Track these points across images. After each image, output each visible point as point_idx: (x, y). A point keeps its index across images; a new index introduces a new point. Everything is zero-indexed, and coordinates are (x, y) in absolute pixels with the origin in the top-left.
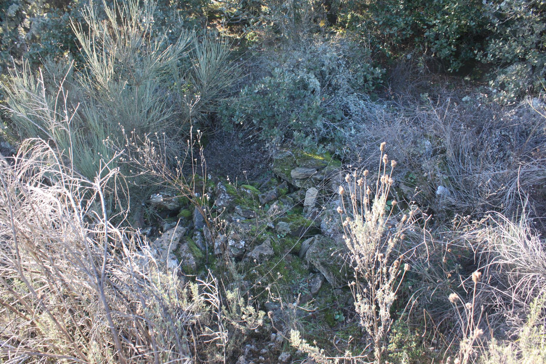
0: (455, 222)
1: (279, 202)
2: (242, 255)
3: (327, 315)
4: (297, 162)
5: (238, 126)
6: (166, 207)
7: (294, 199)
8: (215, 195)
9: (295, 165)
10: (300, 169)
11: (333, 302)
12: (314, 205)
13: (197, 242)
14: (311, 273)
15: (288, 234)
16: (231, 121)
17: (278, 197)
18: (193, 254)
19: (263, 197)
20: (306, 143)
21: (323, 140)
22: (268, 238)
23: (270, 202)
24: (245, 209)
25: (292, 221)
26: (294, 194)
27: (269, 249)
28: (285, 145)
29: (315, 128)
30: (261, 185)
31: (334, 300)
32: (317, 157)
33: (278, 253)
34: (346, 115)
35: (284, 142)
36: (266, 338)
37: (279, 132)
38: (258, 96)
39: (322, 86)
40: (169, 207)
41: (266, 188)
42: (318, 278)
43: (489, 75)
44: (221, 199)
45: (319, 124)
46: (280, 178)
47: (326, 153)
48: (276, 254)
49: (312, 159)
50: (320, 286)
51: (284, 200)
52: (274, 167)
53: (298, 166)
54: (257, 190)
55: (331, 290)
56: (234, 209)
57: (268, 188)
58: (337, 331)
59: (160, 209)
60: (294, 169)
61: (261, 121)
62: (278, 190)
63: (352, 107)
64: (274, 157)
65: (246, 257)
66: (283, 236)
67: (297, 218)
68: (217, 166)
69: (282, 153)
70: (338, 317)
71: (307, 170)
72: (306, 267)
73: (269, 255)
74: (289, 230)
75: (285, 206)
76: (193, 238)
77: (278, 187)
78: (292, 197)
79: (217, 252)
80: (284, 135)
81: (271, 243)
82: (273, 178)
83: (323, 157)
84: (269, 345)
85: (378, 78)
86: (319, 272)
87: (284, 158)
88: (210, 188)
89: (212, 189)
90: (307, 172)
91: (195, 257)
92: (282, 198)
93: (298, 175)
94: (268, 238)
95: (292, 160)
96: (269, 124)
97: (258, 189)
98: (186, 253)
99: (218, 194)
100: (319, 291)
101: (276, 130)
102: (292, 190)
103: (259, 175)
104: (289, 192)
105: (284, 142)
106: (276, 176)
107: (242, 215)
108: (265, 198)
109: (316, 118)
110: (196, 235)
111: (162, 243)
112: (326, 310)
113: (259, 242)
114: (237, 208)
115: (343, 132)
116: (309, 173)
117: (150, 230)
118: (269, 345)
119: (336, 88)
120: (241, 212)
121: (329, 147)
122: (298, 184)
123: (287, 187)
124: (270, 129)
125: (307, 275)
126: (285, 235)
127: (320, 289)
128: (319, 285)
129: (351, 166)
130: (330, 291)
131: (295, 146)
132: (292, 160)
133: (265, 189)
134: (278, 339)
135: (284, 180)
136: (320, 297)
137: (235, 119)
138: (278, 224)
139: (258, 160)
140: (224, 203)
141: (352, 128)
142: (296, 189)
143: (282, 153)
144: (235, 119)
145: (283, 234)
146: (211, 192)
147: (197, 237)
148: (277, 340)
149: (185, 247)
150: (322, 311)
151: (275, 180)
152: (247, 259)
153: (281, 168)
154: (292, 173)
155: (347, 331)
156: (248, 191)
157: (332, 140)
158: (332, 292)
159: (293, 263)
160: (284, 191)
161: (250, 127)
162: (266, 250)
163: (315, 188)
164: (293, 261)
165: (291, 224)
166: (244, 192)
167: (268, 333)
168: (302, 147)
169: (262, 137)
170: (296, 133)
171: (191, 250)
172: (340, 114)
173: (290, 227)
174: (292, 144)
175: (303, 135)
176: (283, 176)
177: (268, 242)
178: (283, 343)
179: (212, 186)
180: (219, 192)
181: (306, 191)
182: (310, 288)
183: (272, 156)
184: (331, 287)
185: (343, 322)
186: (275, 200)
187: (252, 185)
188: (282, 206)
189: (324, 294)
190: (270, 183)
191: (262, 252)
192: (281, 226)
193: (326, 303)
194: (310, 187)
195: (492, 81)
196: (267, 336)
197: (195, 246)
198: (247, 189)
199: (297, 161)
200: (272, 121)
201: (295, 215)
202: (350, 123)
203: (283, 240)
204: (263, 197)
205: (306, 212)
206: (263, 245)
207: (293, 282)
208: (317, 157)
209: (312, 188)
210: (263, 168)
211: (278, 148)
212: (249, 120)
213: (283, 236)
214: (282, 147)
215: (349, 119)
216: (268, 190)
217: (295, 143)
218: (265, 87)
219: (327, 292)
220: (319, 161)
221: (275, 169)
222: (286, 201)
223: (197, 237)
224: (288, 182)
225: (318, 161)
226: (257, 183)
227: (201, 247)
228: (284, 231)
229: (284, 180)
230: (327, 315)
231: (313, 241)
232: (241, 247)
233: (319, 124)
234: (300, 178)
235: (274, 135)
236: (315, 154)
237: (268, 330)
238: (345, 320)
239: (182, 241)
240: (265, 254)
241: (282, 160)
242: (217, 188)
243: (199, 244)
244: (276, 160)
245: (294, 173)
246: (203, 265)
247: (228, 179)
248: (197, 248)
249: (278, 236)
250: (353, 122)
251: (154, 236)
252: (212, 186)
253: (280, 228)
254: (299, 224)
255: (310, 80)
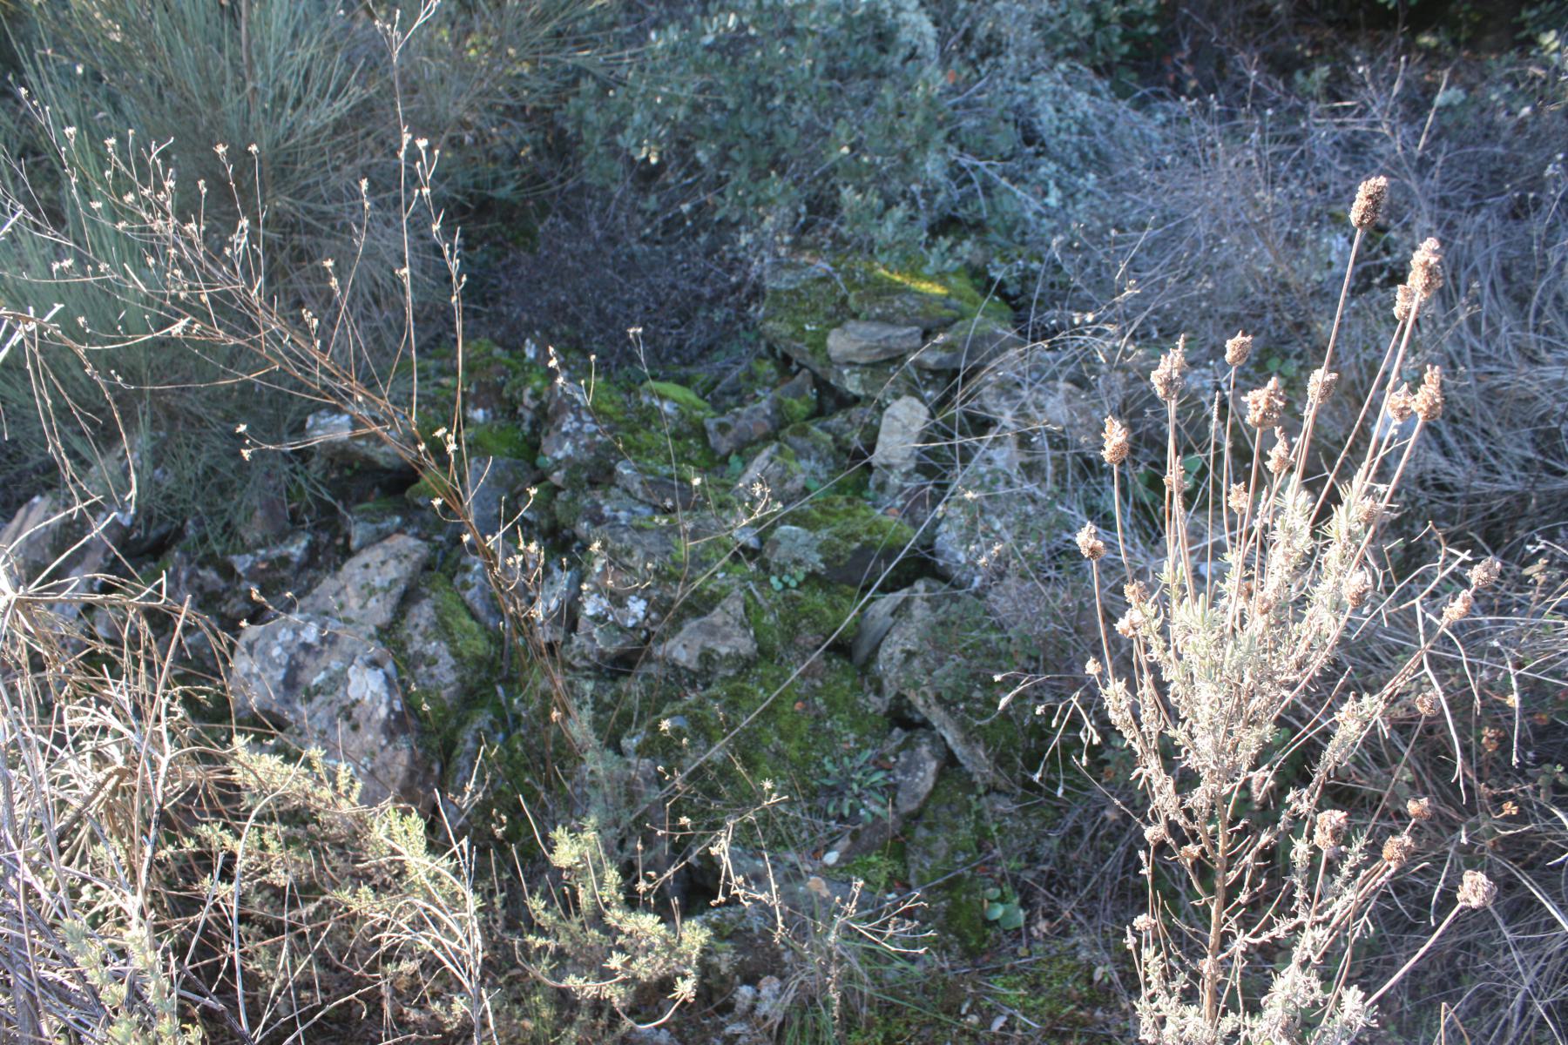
0: (1541, 579)
1: (780, 451)
2: (639, 652)
3: (956, 904)
4: (852, 301)
5: (647, 176)
6: (368, 461)
7: (835, 440)
8: (545, 415)
9: (842, 314)
10: (862, 328)
11: (980, 849)
12: (912, 464)
13: (468, 595)
14: (897, 731)
15: (812, 576)
16: (615, 152)
17: (779, 428)
18: (452, 642)
19: (723, 428)
20: (887, 230)
21: (947, 225)
22: (736, 591)
23: (746, 449)
24: (652, 472)
25: (828, 525)
26: (838, 419)
27: (737, 631)
28: (808, 239)
29: (916, 180)
30: (715, 384)
31: (982, 841)
32: (925, 287)
33: (773, 648)
34: (1029, 141)
35: (805, 228)
36: (719, 1001)
37: (785, 190)
38: (713, 58)
39: (942, 39)
40: (382, 461)
41: (733, 393)
42: (924, 750)
43: (1534, 13)
44: (567, 434)
45: (933, 166)
46: (787, 359)
47: (956, 273)
48: (765, 653)
49: (907, 291)
50: (930, 782)
51: (798, 442)
52: (766, 318)
53: (855, 316)
54: (700, 403)
55: (972, 798)
56: (611, 471)
57: (740, 394)
58: (998, 971)
59: (351, 467)
60: (839, 325)
61: (724, 158)
62: (780, 402)
63: (1047, 117)
64: (770, 284)
65: (649, 659)
66: (793, 583)
67: (849, 513)
68: (557, 309)
69: (796, 267)
70: (998, 912)
71: (889, 331)
72: (876, 704)
73: (739, 657)
74: (815, 561)
75: (803, 463)
76: (457, 580)
77: (777, 393)
78: (828, 430)
79: (544, 636)
80: (808, 203)
81: (746, 609)
82: (760, 357)
83: (944, 283)
84: (728, 1031)
85: (1143, 17)
86: (926, 724)
87: (805, 287)
88: (528, 391)
89: (536, 395)
90: (887, 338)
91: (457, 655)
92: (793, 433)
93: (853, 348)
94: (736, 591)
95: (832, 293)
96: (754, 163)
97: (702, 397)
98: (426, 637)
99: (556, 413)
100: (926, 803)
101: (775, 185)
102: (830, 402)
103: (710, 347)
104: (819, 412)
105: (805, 228)
106: (771, 349)
107: (640, 495)
108: (730, 434)
109: (923, 143)
110: (467, 569)
111: (343, 598)
112: (951, 885)
113: (701, 604)
114: (624, 470)
115: (1021, 201)
116: (894, 344)
117: (304, 543)
118: (728, 1031)
119: (993, 47)
120: (637, 486)
121: (967, 248)
122: (852, 384)
123: (812, 393)
124: (756, 181)
125: (884, 734)
126: (801, 577)
127: (931, 794)
128: (925, 777)
129: (1090, 317)
130: (969, 805)
131: (846, 243)
132: (832, 293)
133: (731, 400)
134: (764, 1008)
135: (801, 367)
136: (929, 827)
137: (625, 140)
138: (776, 534)
139: (707, 291)
140: (576, 447)
141: (1051, 183)
142: (846, 402)
143: (796, 267)
144: (625, 140)
145: (793, 576)
146: (533, 405)
147: (469, 577)
148: (760, 1012)
149: (423, 613)
150: (939, 887)
151: (767, 368)
152: (653, 669)
153: (794, 322)
154: (831, 342)
155: (1037, 977)
156: (667, 407)
157: (979, 227)
158: (976, 807)
159: (826, 686)
160: (800, 407)
161: (686, 176)
162: (726, 637)
163: (915, 402)
164: (830, 679)
165: (824, 534)
166: (651, 407)
167: (723, 979)
168: (868, 248)
169: (726, 209)
170: (848, 195)
171: (443, 629)
172: (1006, 138)
173: (820, 549)
174: (833, 236)
175: (876, 202)
176: (799, 349)
177: (735, 606)
178: (782, 1025)
179: (538, 383)
180: (561, 409)
181: (881, 409)
182: (891, 791)
183: (760, 277)
184: (971, 787)
185: (1017, 934)
186: (767, 439)
187: (684, 382)
188: (793, 465)
189: (944, 813)
190: (752, 377)
191: (711, 644)
192: (786, 544)
193: (954, 851)
194: (897, 397)
195: (1553, 34)
196: (721, 993)
197: (463, 613)
198: (662, 398)
199: (852, 296)
200: (764, 154)
201: (841, 499)
202: (1043, 170)
203: (794, 599)
204: (723, 428)
205: (882, 487)
206: (716, 616)
207: (829, 767)
208: (925, 287)
209: (905, 400)
210: (726, 322)
211: (782, 251)
212: (682, 146)
213: (793, 583)
214: (797, 246)
215: (1038, 154)
216: (741, 403)
217: (844, 230)
218: (741, 27)
219: (956, 808)
220: (932, 298)
221: (770, 324)
222: (808, 444)
223: (469, 577)
224: (814, 375)
225: (924, 298)
226: (702, 374)
227: (482, 613)
228: (798, 562)
229: (801, 367)
230: (956, 904)
231: (907, 602)
232: (630, 623)
233: (933, 166)
234: (863, 360)
235: (770, 201)
236: (916, 274)
237: (724, 969)
238: (1028, 926)
239: (408, 598)
240: (724, 650)
241: (796, 292)
242: (552, 393)
243: (478, 606)
244: (775, 291)
245: (838, 343)
246: (488, 684)
247: (553, 363)
248: (467, 621)
249: (774, 580)
250: (1052, 167)
251: (319, 568)
252: (538, 383)
253: (782, 551)
254: (853, 536)
255: (903, 16)
